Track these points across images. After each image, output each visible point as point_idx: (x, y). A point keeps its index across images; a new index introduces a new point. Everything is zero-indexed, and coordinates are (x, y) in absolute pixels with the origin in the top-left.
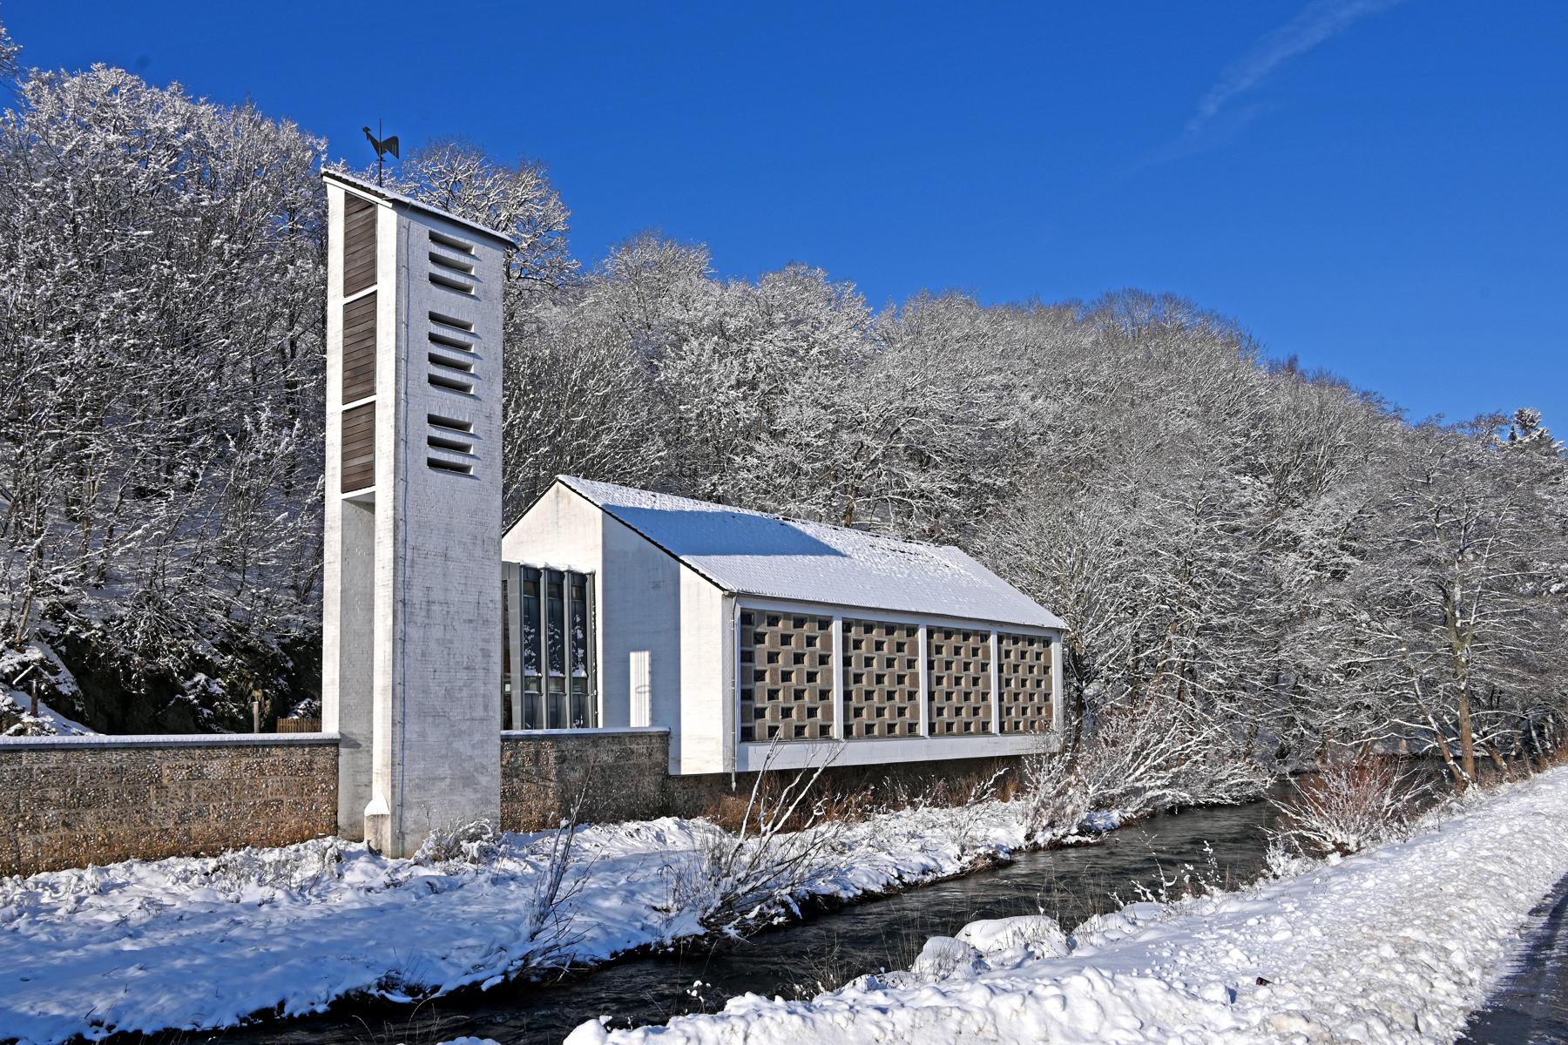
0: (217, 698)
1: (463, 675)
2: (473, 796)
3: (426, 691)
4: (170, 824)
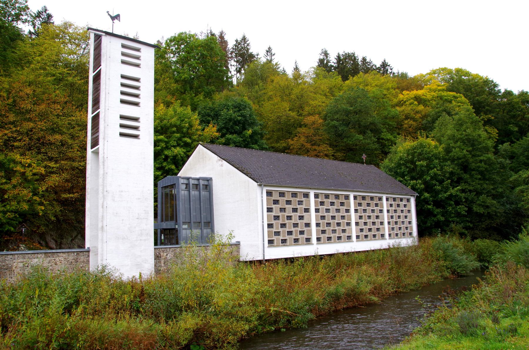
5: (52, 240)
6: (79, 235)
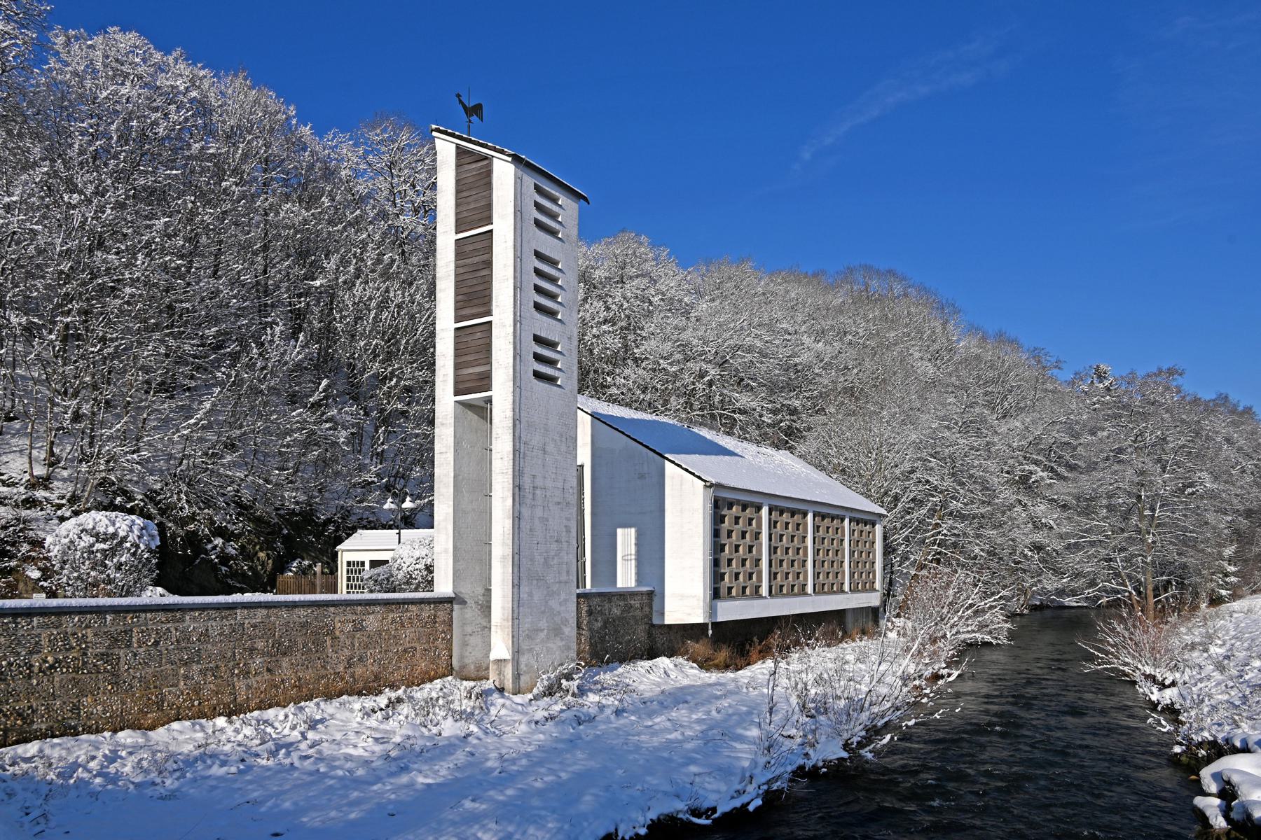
0: (232, 557)
1: (554, 546)
3: (532, 560)
4: (341, 669)
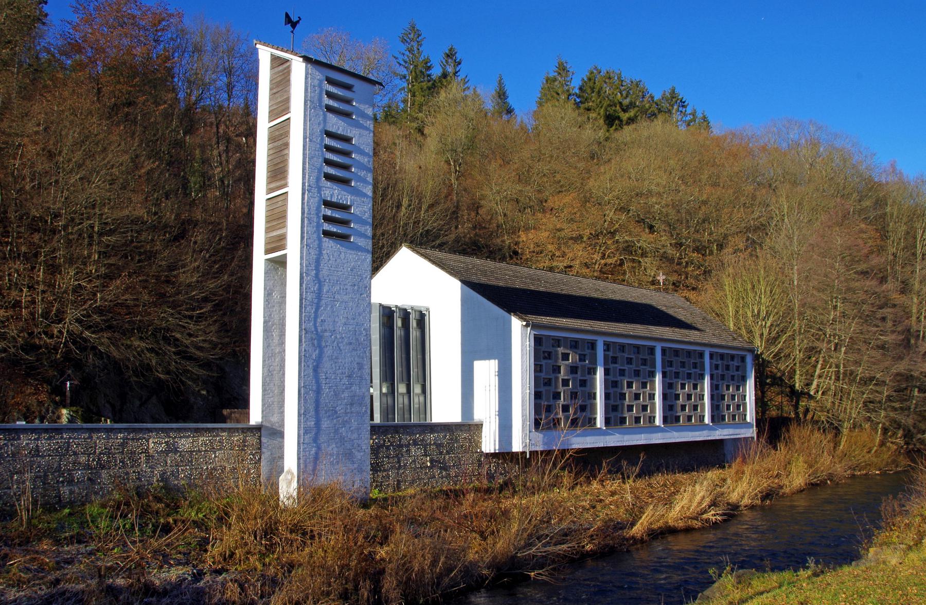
2: (351, 466)
5: (106, 405)
6: (154, 397)
